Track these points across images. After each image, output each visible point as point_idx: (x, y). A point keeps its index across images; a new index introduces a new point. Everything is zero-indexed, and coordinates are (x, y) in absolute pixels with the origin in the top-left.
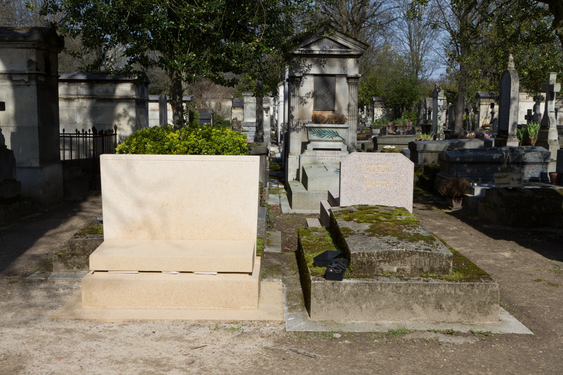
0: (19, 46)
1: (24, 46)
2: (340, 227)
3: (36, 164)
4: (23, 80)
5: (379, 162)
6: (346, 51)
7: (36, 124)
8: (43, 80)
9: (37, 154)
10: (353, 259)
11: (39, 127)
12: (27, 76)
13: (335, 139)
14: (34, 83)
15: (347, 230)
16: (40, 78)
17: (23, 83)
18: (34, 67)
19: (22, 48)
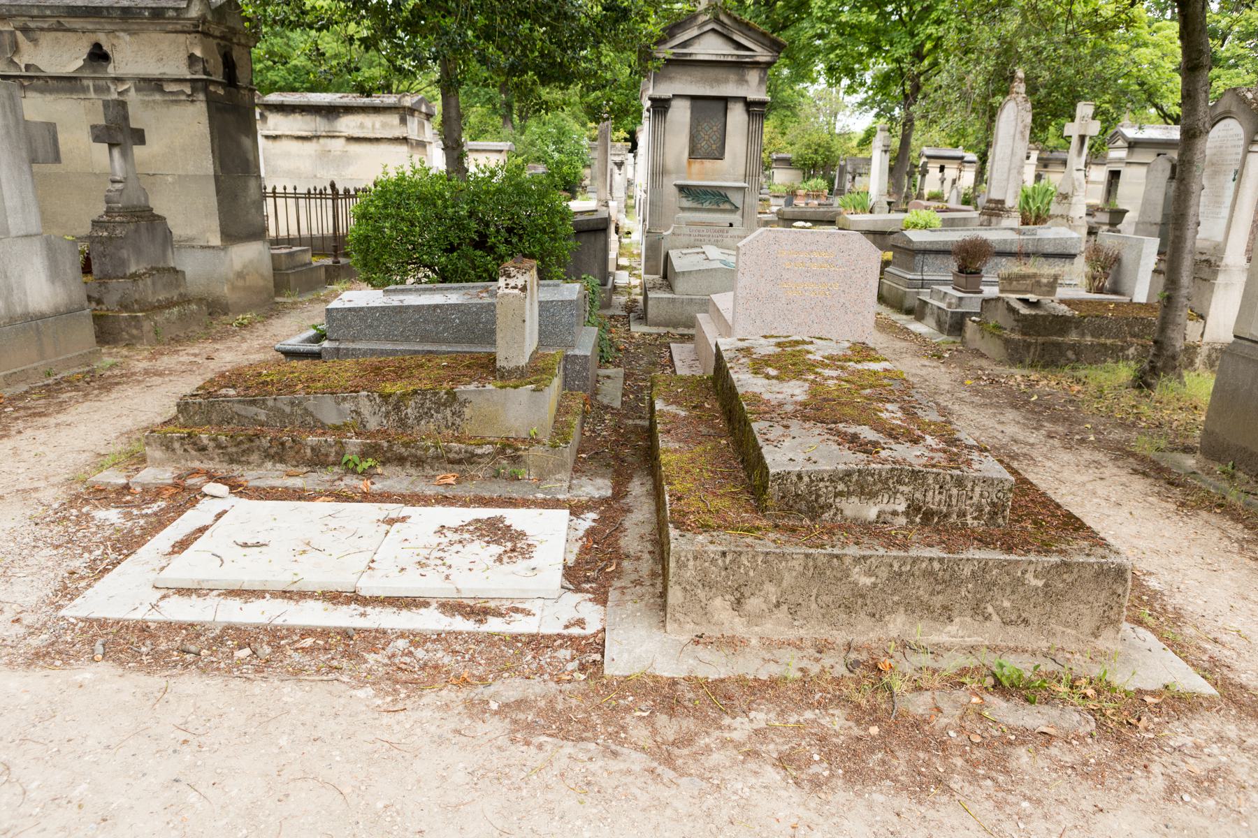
0: (170, 27)
1: (179, 27)
2: (740, 391)
3: (216, 240)
4: (182, 92)
5: (814, 248)
6: (747, 56)
7: (211, 172)
8: (221, 92)
9: (215, 224)
10: (773, 489)
11: (216, 177)
12: (189, 84)
13: (722, 207)
14: (201, 96)
15: (756, 399)
16: (212, 88)
17: (183, 98)
18: (199, 67)
19: (176, 32)
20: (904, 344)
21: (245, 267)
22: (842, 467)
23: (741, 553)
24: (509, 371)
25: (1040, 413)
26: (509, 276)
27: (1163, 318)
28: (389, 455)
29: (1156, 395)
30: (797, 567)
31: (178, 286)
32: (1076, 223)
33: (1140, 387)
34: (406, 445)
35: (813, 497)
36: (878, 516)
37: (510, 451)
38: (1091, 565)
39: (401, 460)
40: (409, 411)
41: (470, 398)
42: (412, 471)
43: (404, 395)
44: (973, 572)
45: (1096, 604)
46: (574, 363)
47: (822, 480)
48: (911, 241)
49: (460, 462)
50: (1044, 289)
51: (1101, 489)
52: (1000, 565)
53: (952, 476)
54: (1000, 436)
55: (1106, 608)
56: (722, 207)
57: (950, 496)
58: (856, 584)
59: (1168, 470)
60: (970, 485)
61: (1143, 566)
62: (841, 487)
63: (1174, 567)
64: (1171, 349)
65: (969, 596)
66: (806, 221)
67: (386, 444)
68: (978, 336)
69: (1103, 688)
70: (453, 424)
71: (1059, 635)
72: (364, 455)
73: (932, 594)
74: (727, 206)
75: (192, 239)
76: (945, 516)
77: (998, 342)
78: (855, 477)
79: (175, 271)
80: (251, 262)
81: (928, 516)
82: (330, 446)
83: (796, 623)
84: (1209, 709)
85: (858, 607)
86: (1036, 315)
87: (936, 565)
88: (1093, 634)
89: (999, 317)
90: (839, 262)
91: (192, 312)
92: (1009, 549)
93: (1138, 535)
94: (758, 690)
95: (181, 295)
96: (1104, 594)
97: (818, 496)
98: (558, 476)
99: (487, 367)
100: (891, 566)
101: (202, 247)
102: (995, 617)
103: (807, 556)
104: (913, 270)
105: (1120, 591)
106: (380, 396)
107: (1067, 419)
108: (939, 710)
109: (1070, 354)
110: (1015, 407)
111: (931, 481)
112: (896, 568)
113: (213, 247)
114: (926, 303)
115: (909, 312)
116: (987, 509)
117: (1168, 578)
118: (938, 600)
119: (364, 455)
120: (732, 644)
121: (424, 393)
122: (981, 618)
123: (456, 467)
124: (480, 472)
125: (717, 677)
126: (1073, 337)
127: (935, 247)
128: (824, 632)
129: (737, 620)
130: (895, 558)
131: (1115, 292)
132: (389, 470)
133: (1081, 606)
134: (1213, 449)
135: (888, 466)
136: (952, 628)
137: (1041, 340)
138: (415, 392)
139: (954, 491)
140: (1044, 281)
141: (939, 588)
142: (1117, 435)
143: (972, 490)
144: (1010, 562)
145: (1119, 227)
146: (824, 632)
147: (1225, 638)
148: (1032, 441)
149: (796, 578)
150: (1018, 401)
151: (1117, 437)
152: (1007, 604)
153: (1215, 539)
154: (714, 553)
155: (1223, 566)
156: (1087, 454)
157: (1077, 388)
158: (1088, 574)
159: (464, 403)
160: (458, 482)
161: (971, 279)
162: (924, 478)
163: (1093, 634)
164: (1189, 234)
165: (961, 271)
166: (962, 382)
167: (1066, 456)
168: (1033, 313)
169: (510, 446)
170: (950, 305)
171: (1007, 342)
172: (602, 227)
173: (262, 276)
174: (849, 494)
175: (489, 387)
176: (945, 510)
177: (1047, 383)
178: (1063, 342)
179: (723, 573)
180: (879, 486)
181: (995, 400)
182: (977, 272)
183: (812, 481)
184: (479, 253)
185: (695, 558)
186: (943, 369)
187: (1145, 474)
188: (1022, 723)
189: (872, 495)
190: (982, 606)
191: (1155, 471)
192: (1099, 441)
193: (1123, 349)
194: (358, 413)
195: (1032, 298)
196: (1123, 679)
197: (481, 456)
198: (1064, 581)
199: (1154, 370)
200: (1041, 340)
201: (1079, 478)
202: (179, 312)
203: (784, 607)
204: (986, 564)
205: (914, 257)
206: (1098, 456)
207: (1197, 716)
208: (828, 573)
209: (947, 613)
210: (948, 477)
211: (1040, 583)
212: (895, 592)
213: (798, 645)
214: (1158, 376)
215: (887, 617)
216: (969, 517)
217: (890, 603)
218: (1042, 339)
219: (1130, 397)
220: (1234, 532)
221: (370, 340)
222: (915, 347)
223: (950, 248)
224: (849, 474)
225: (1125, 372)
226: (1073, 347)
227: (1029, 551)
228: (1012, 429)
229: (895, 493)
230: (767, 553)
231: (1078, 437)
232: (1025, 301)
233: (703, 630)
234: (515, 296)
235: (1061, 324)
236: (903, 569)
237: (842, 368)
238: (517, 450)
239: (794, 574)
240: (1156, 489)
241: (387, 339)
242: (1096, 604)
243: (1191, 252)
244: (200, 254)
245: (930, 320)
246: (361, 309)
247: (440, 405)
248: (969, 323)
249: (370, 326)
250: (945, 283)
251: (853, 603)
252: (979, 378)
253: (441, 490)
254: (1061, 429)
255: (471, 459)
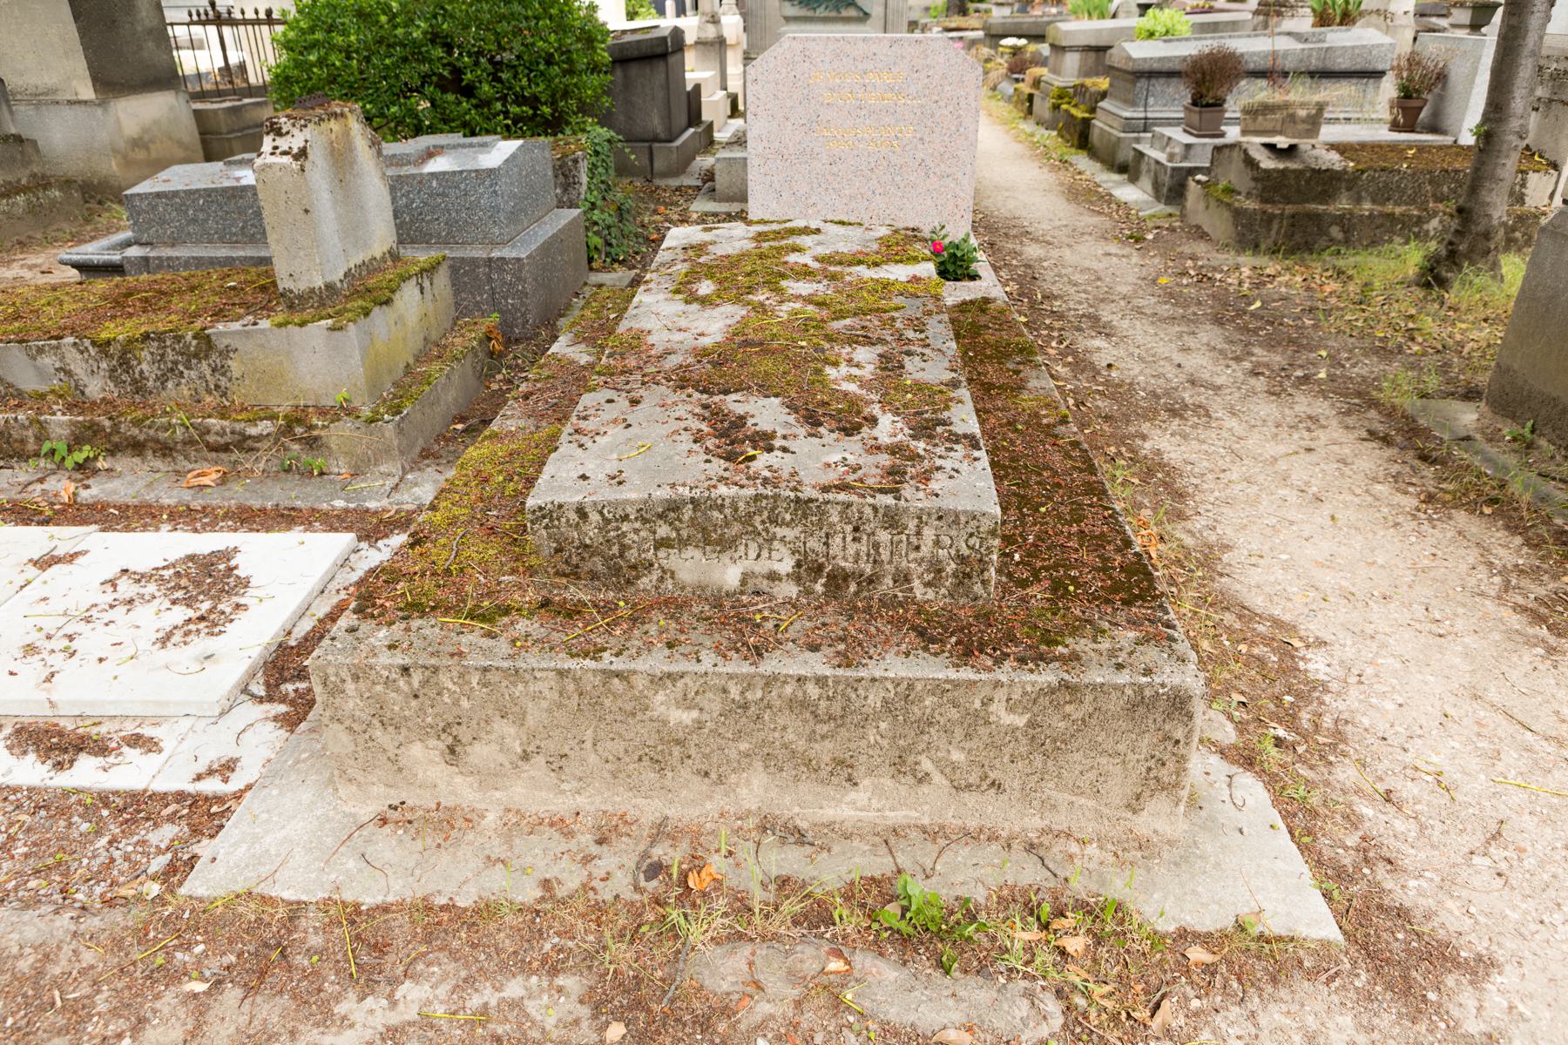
3: (87, 92)
9: (80, 66)
13: (845, 13)
20: (1096, 220)
21: (145, 130)
22: (664, 493)
23: (436, 670)
24: (300, 297)
25: (1255, 331)
26: (279, 133)
27: (1476, 170)
28: (116, 439)
29: (1451, 297)
30: (546, 692)
31: (26, 163)
32: (1397, 22)
33: (1428, 285)
34: (137, 423)
35: (615, 549)
36: (744, 582)
37: (301, 428)
38: (1120, 689)
39: (137, 448)
40: (144, 366)
41: (234, 344)
42: (158, 464)
43: (130, 341)
44: (885, 701)
45: (1130, 756)
46: (501, 270)
47: (625, 518)
48: (1129, 58)
49: (225, 448)
50: (1301, 127)
51: (1301, 469)
52: (938, 688)
53: (875, 509)
54: (1170, 371)
55: (1152, 763)
56: (845, 13)
57: (876, 546)
58: (665, 723)
59: (1426, 433)
60: (912, 525)
61: (1312, 627)
62: (663, 531)
63: (1369, 629)
64: (1484, 221)
65: (885, 743)
66: (1020, 37)
67: (107, 423)
68: (1202, 206)
69: (1106, 921)
70: (217, 387)
71: (1063, 808)
72: (76, 442)
73: (811, 738)
74: (852, 12)
75: (55, 91)
76: (870, 581)
77: (1227, 214)
78: (687, 513)
79: (19, 139)
80: (156, 122)
81: (838, 580)
82: (23, 427)
83: (565, 786)
84: (1312, 975)
85: (675, 761)
86: (1284, 172)
87: (813, 691)
88: (1128, 806)
89: (1234, 175)
90: (912, 90)
91: (53, 202)
92: (967, 653)
93: (1329, 563)
94: (441, 926)
95: (34, 176)
96: (1145, 743)
97: (624, 548)
98: (382, 469)
99: (262, 293)
100: (725, 691)
101: (70, 103)
102: (937, 778)
103: (561, 673)
104: (1132, 103)
105: (1179, 734)
106: (94, 343)
107: (1296, 343)
108: (759, 986)
109: (1335, 232)
110: (1218, 321)
111: (835, 518)
112: (734, 692)
113: (86, 102)
114: (1141, 155)
115: (1122, 169)
116: (951, 567)
117: (1350, 652)
118: (824, 751)
119: (76, 442)
120: (446, 823)
121: (160, 337)
122: (909, 779)
123: (223, 456)
124: (258, 464)
125: (379, 899)
126: (1343, 204)
127: (1167, 66)
128: (620, 801)
129: (459, 779)
130: (731, 677)
131: (1434, 129)
132: (123, 463)
133: (1103, 760)
134: (1507, 399)
135: (750, 492)
136: (860, 796)
137: (1290, 209)
138: (146, 337)
139: (884, 536)
140: (1302, 113)
141: (823, 729)
142: (1366, 367)
143: (918, 533)
144: (957, 684)
145: (1483, 30)
146: (620, 801)
147: (1406, 790)
148: (1219, 381)
149: (549, 711)
150: (1229, 312)
151: (1364, 371)
152: (957, 756)
153: (1463, 568)
154: (388, 668)
155: (1460, 625)
156: (1304, 403)
157: (1333, 286)
158: (1114, 704)
159: (226, 352)
160: (224, 480)
161: (1209, 114)
162: (823, 513)
163: (1128, 806)
164: (1534, 21)
165: (1194, 104)
166: (1154, 281)
167: (1266, 409)
168: (1281, 166)
169: (299, 421)
170: (1171, 157)
171: (1238, 214)
172: (659, 50)
173: (180, 143)
174: (683, 543)
175: (265, 324)
176: (868, 570)
177: (1288, 280)
178: (1325, 213)
179: (414, 703)
180: (736, 528)
181: (1194, 309)
182: (1219, 104)
183: (607, 521)
184: (450, 97)
185: (356, 678)
186: (1135, 259)
187: (1386, 441)
188: (912, 1018)
189: (726, 545)
190: (911, 759)
191: (1408, 438)
192: (1332, 378)
193: (1420, 221)
194: (69, 373)
195: (1282, 142)
196: (1164, 904)
197: (259, 438)
198: (1066, 717)
199: (1453, 257)
200: (1290, 209)
201: (1272, 449)
202: (29, 202)
203: (540, 760)
204: (910, 687)
205: (1134, 83)
206: (1322, 408)
207: (1283, 993)
208: (607, 702)
209: (845, 771)
210: (868, 511)
211: (1021, 721)
212: (739, 735)
213: (562, 826)
214: (1460, 268)
215: (733, 778)
216: (916, 583)
217: (733, 754)
218: (1295, 208)
219: (1407, 301)
220: (1502, 552)
221: (198, 242)
222: (1108, 224)
223: (1177, 67)
224: (673, 507)
225: (1413, 257)
226: (1340, 220)
227: (998, 662)
228: (1199, 362)
229: (770, 541)
230: (486, 670)
231: (1299, 373)
232: (1271, 147)
233: (404, 797)
234: (282, 168)
235: (1325, 182)
236: (749, 695)
237: (833, 277)
238: (312, 427)
239: (544, 704)
240: (1395, 469)
241: (222, 240)
242: (1130, 756)
243: (1533, 54)
244: (68, 113)
245: (1146, 182)
246: (175, 194)
247: (191, 357)
248: (1191, 184)
249: (194, 221)
250: (1169, 122)
251: (664, 753)
252: (1184, 274)
253: (187, 496)
254: (1277, 359)
255: (244, 443)
